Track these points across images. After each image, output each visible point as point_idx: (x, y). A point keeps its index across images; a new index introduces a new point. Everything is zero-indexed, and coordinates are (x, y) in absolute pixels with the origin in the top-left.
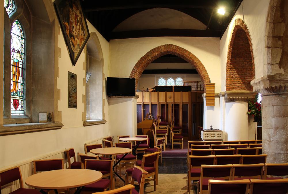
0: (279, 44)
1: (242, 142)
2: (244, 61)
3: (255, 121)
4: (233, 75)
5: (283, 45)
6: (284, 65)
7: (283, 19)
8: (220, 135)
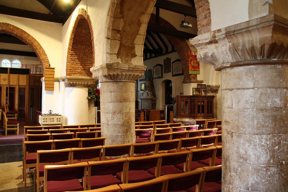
0: (118, 37)
1: (82, 126)
2: (86, 49)
3: (95, 106)
4: (73, 61)
5: (121, 38)
6: (122, 56)
7: (122, 16)
8: (60, 120)
